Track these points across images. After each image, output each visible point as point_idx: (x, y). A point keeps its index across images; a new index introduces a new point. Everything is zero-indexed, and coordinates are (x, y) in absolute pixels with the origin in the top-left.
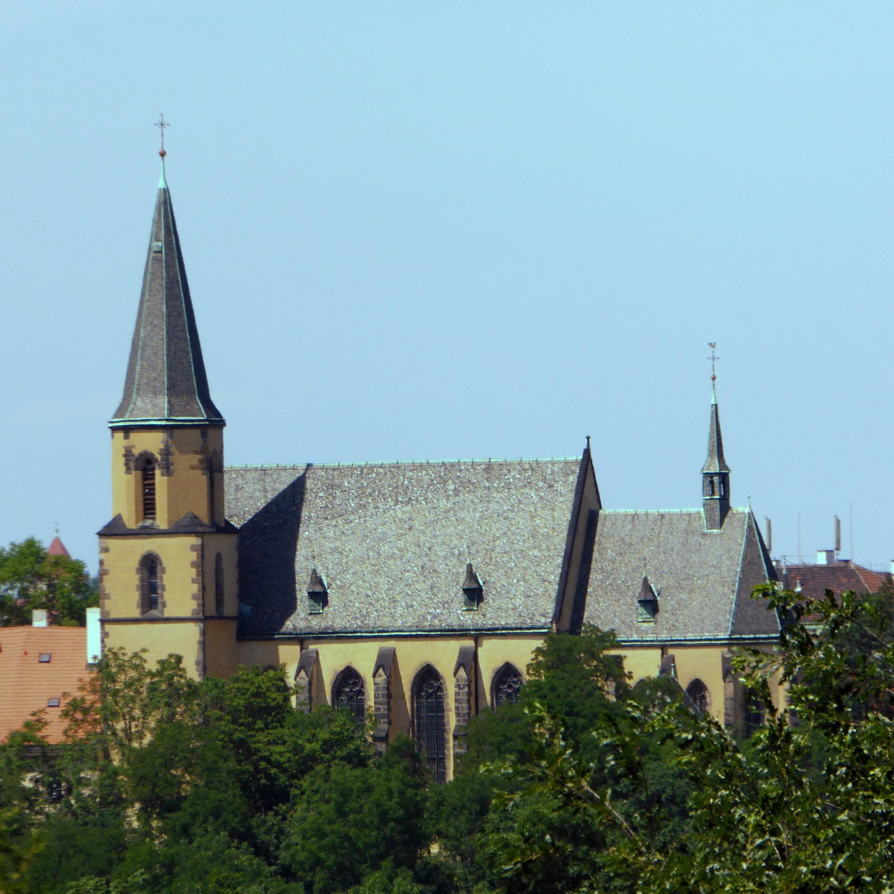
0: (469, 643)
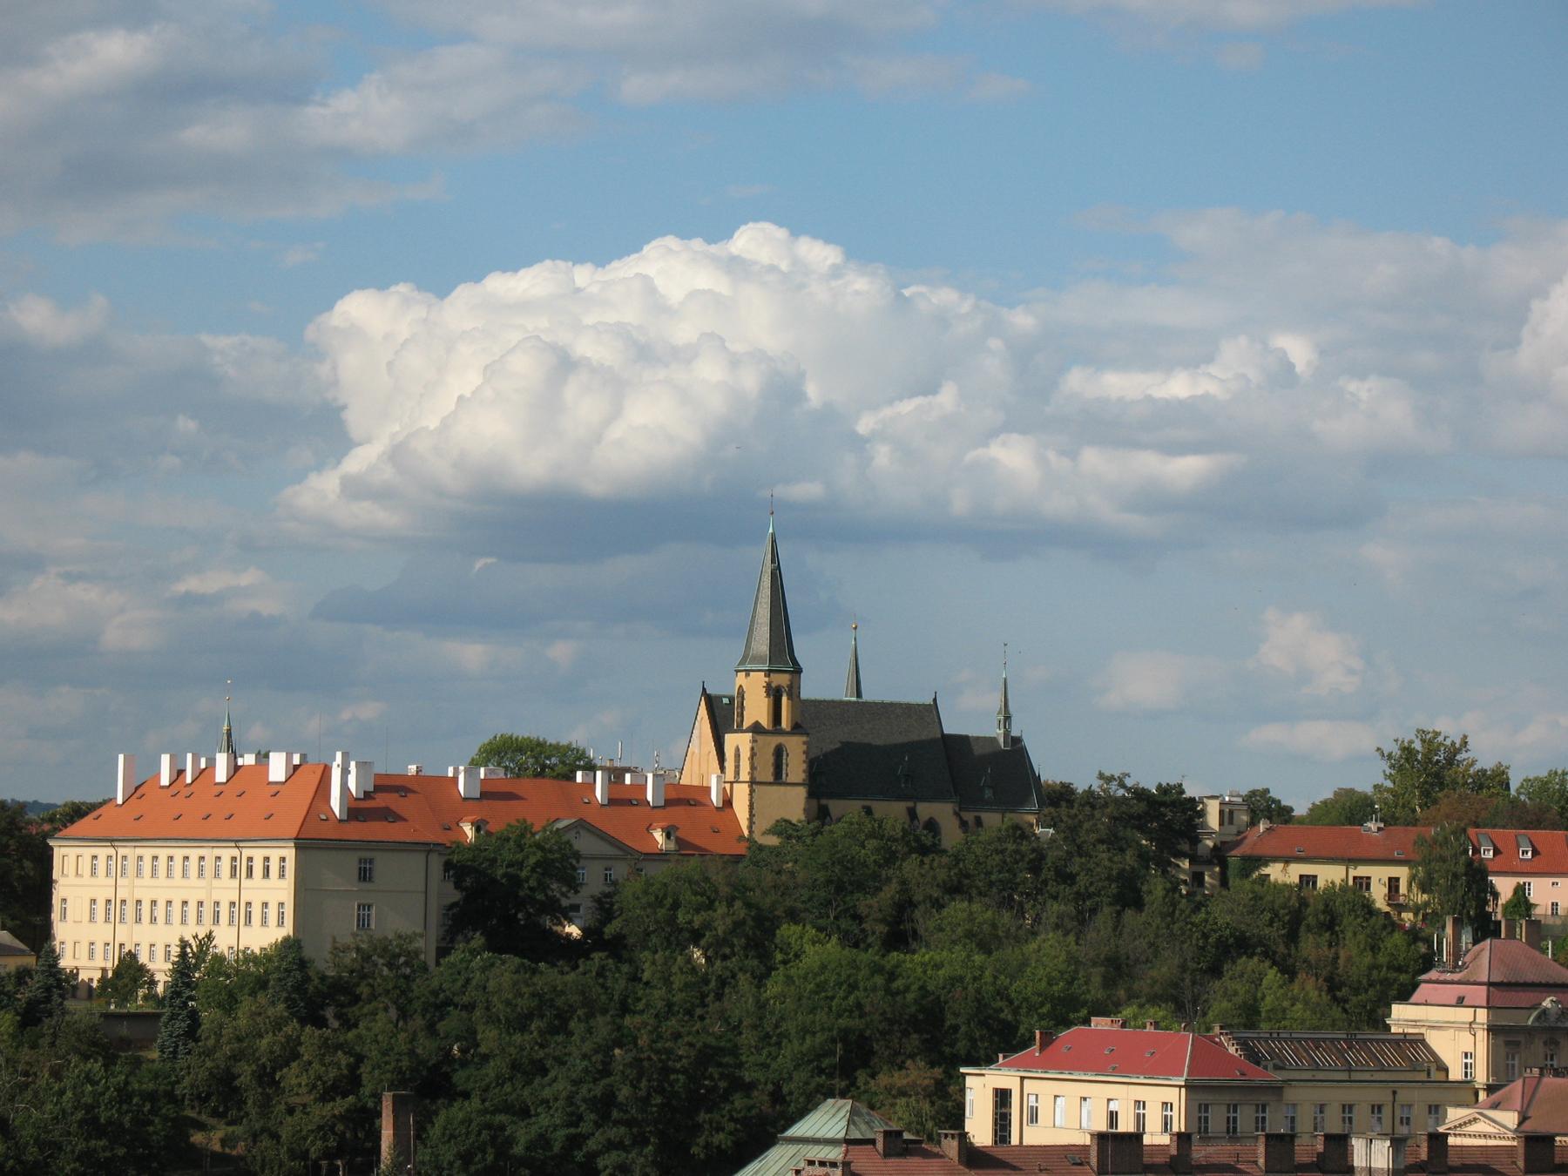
0: (910, 804)
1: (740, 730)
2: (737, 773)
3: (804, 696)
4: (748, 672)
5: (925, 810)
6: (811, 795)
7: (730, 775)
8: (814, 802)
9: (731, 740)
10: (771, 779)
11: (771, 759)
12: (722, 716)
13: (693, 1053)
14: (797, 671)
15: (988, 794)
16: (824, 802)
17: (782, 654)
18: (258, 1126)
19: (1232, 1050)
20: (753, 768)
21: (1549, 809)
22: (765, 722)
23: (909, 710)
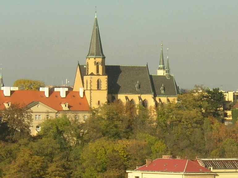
0: (139, 95)
1: (88, 75)
2: (87, 87)
3: (106, 64)
4: (89, 58)
5: (144, 97)
6: (109, 93)
7: (85, 89)
8: (110, 96)
9: (85, 77)
10: (97, 89)
11: (97, 83)
12: (83, 72)
13: (71, 154)
14: (104, 58)
15: (163, 92)
16: (113, 95)
17: (99, 51)
18: (25, 156)
19: (138, 82)
20: (91, 86)
21: (231, 138)
22: (95, 73)
23: (140, 68)
